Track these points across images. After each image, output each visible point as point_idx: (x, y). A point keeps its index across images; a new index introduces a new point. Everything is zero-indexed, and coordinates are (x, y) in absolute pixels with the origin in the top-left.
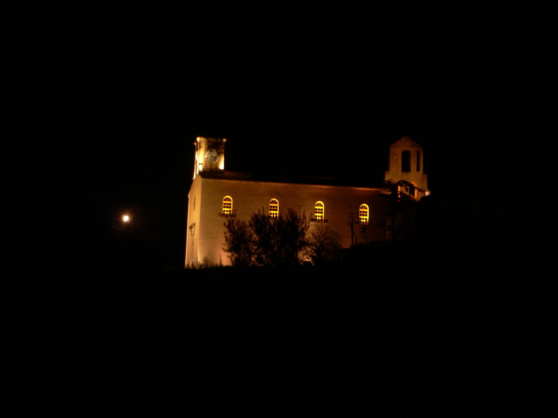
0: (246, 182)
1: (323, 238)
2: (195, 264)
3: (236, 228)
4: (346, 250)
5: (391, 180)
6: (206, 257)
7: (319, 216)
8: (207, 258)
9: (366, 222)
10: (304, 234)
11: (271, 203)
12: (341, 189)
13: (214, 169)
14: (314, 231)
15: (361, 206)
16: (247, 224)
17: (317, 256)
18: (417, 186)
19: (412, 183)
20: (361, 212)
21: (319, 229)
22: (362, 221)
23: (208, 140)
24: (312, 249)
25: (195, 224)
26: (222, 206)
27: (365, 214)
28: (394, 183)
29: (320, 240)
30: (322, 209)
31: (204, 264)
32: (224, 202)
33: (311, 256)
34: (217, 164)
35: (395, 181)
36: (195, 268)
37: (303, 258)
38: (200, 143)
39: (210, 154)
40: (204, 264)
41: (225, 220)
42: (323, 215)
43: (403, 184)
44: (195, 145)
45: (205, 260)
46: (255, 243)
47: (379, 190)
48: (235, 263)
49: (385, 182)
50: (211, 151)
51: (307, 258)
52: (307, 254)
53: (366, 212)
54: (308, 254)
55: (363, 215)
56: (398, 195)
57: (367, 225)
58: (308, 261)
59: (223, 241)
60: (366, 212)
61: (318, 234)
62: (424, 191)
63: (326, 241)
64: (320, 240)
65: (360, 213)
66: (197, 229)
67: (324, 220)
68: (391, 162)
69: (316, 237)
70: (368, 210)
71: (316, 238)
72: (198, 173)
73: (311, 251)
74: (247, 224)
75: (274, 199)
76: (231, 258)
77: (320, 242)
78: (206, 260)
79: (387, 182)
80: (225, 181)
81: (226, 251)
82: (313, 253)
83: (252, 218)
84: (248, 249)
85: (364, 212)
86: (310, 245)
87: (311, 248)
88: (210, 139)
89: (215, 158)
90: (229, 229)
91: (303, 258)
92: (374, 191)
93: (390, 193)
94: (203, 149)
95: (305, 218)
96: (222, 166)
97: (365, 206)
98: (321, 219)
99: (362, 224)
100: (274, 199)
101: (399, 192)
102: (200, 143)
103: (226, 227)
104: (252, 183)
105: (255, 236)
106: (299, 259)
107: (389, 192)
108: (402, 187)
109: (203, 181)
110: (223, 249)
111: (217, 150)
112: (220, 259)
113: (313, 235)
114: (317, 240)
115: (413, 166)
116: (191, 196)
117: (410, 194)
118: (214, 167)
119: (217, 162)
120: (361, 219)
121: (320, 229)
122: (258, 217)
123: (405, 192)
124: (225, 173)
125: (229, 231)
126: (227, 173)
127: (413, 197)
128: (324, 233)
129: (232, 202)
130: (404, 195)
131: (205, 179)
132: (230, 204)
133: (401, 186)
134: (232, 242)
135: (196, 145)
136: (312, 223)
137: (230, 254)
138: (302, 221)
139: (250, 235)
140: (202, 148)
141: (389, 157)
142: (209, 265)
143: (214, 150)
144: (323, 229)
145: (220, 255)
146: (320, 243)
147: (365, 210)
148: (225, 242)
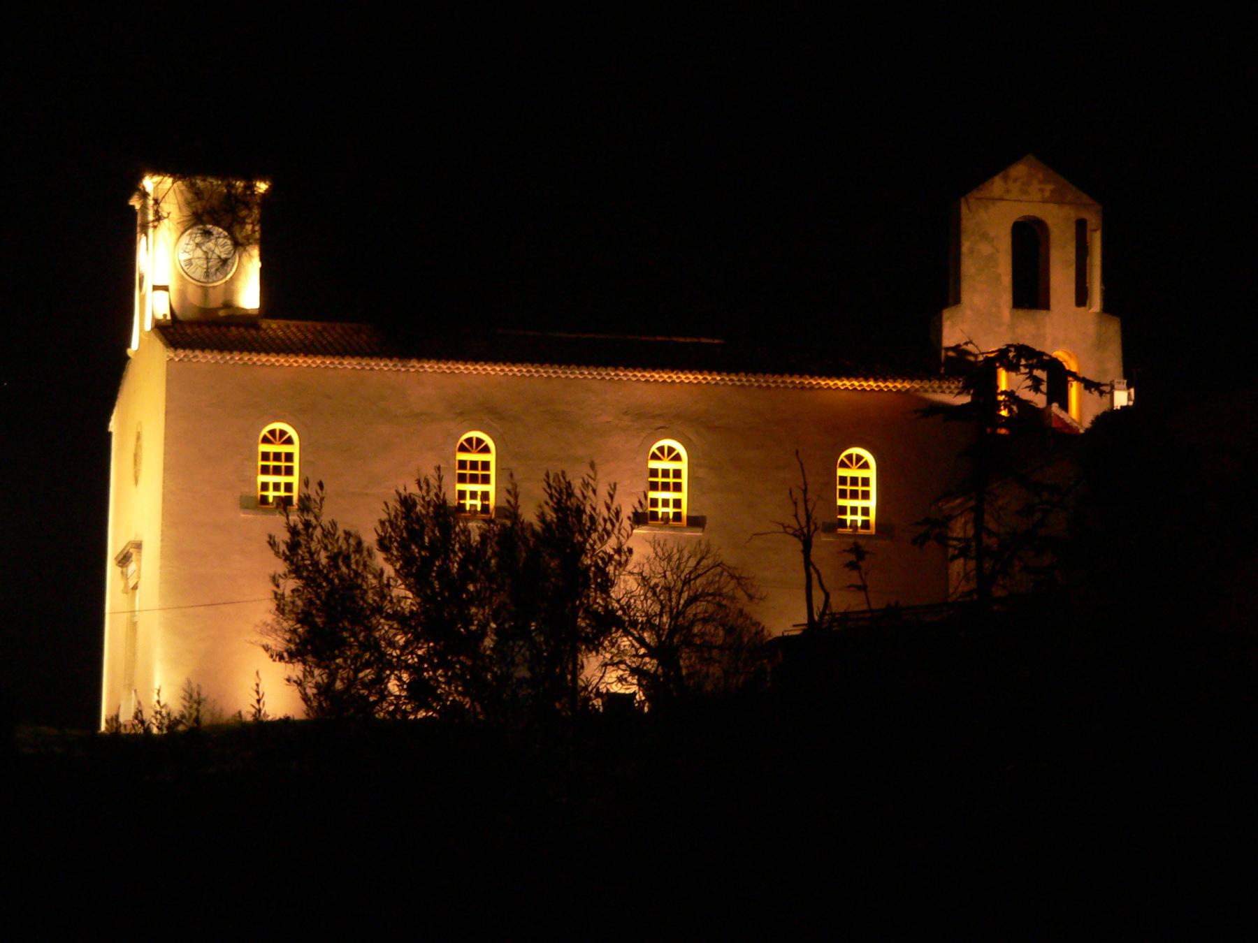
0: (354, 362)
1: (685, 595)
2: (148, 715)
3: (323, 558)
4: (784, 640)
5: (966, 344)
6: (194, 686)
7: (666, 503)
8: (199, 686)
9: (866, 524)
10: (606, 584)
11: (463, 449)
12: (760, 387)
13: (217, 309)
14: (647, 566)
15: (842, 456)
16: (370, 539)
17: (660, 670)
18: (1079, 367)
19: (1059, 354)
20: (843, 480)
21: (669, 558)
22: (849, 518)
23: (192, 186)
24: (641, 641)
25: (138, 546)
26: (257, 465)
27: (860, 488)
28: (981, 358)
29: (674, 601)
30: (677, 473)
31: (187, 715)
32: (264, 448)
33: (634, 671)
34: (230, 287)
35: (984, 349)
36: (148, 730)
37: (602, 678)
38: (156, 202)
39: (198, 245)
40: (187, 715)
41: (277, 526)
42: (683, 496)
43: (1019, 361)
44: (133, 206)
45: (191, 697)
46: (402, 620)
47: (917, 385)
48: (315, 704)
49: (943, 353)
50: (207, 234)
51: (621, 679)
52: (617, 664)
53: (866, 482)
54: (622, 662)
55: (854, 495)
56: (997, 405)
57: (869, 537)
58: (622, 691)
59: (263, 610)
60: (866, 482)
61: (665, 576)
62: (1107, 389)
63: (700, 607)
64: (674, 601)
65: (839, 487)
66: (149, 566)
67: (688, 517)
68: (968, 267)
69: (653, 589)
70: (872, 474)
71: (654, 594)
72: (148, 326)
73: (637, 650)
74: (370, 539)
75: (278, 426)
76: (299, 684)
77: (671, 612)
78: (194, 698)
79: (951, 354)
80: (264, 358)
81: (281, 658)
82: (644, 656)
83: (393, 514)
84: (372, 645)
85: (854, 481)
86: (627, 626)
87: (633, 636)
88: (200, 183)
89: (224, 262)
90: (292, 563)
91: (602, 678)
92: (899, 391)
93: (966, 399)
94: (172, 226)
95: (617, 514)
96: (249, 296)
97: (859, 458)
98: (675, 514)
99: (849, 530)
100: (666, 443)
101: (1003, 393)
102: (156, 202)
103: (277, 553)
104: (384, 367)
105: (400, 590)
106: (586, 688)
107: (959, 394)
108: (1013, 374)
109: (171, 359)
110: (266, 648)
111: (228, 229)
112: (258, 692)
113: (644, 580)
114: (661, 602)
115: (1061, 280)
116: (121, 424)
117: (1049, 402)
118: (216, 301)
119: (231, 278)
120: (843, 510)
121: (669, 558)
122: (415, 504)
123: (1027, 395)
124: (264, 324)
125: (290, 572)
126: (273, 326)
127: (1062, 414)
128: (690, 573)
129: (295, 449)
130: (1025, 405)
131: (181, 353)
132: (289, 457)
133: (1012, 367)
134: (304, 618)
135: (138, 207)
136: (640, 531)
137: (296, 670)
138: (600, 529)
139: (381, 587)
140: (166, 221)
141: (958, 246)
142: (206, 719)
143: (220, 230)
144: (686, 554)
145: (257, 673)
146: (671, 618)
147: (860, 474)
148: (270, 618)
